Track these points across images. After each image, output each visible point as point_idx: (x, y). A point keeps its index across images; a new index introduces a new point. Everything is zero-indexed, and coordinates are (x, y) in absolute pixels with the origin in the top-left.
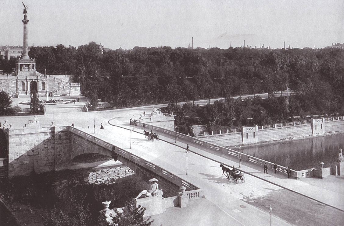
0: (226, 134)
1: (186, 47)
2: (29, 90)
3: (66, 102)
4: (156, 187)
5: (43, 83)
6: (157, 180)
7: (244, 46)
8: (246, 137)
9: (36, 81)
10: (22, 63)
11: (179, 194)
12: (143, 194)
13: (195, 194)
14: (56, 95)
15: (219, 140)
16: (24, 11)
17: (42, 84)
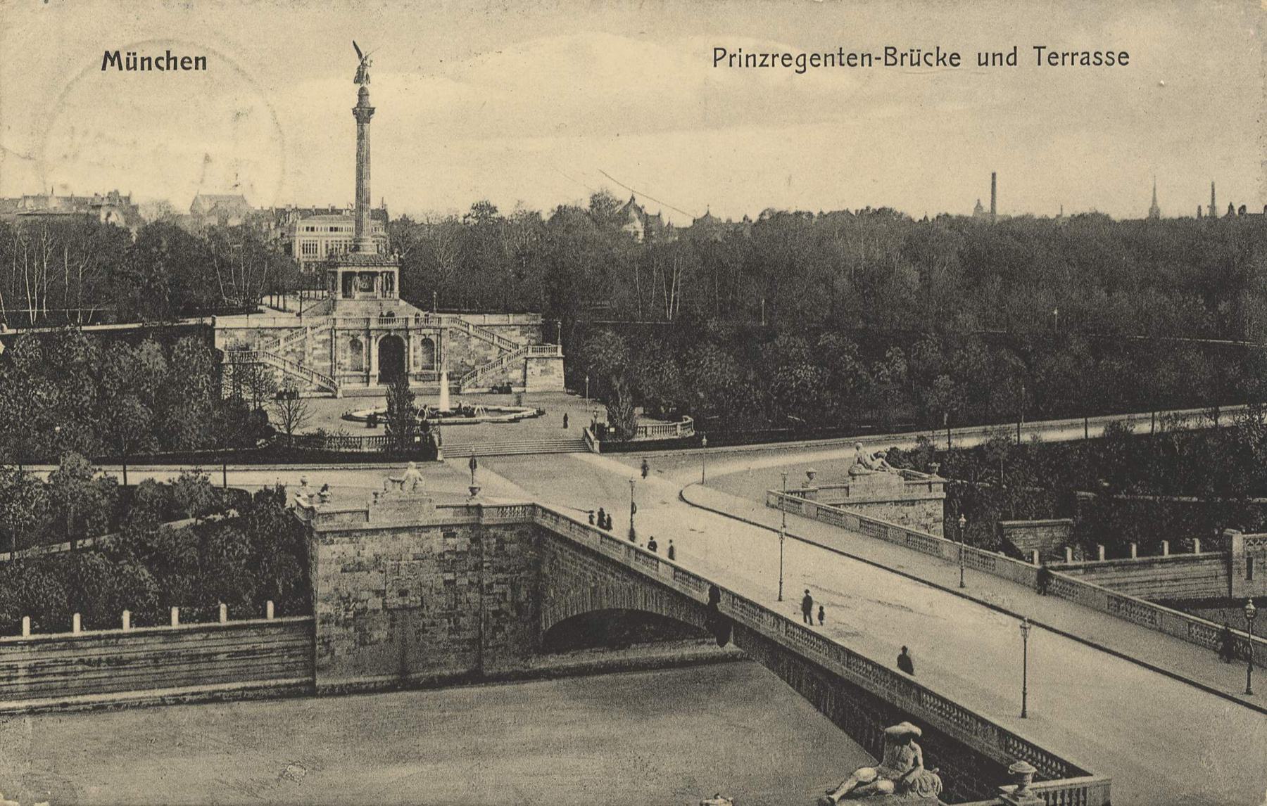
0: (1159, 557)
1: (968, 211)
2: (375, 370)
3: (512, 416)
4: (916, 759)
5: (427, 343)
6: (917, 730)
7: (1213, 207)
8: (1245, 574)
9: (400, 334)
10: (349, 269)
11: (1004, 792)
12: (860, 784)
13: (1070, 796)
14: (477, 391)
15: (1129, 580)
16: (359, 72)
17: (420, 349)
